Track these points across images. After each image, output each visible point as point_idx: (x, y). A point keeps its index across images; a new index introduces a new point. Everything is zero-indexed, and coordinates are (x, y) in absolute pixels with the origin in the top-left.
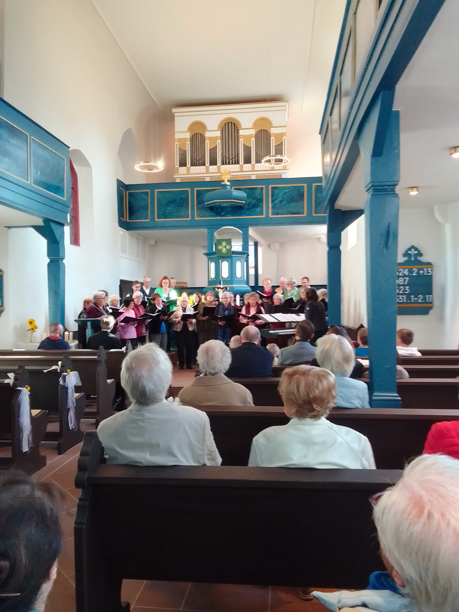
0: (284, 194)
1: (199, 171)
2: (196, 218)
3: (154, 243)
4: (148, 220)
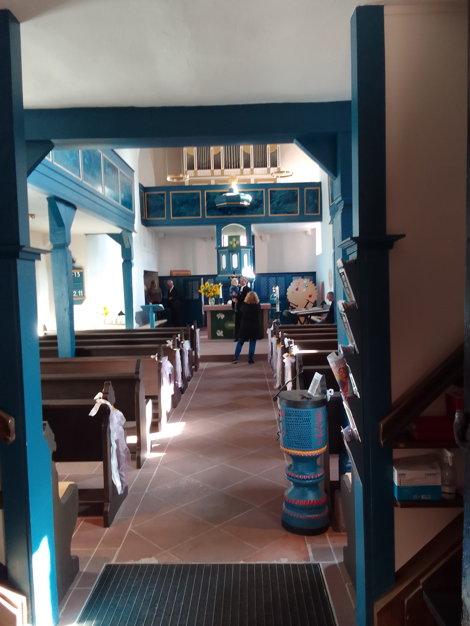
0: (281, 196)
1: (207, 174)
2: (206, 217)
3: (163, 236)
4: (165, 218)
